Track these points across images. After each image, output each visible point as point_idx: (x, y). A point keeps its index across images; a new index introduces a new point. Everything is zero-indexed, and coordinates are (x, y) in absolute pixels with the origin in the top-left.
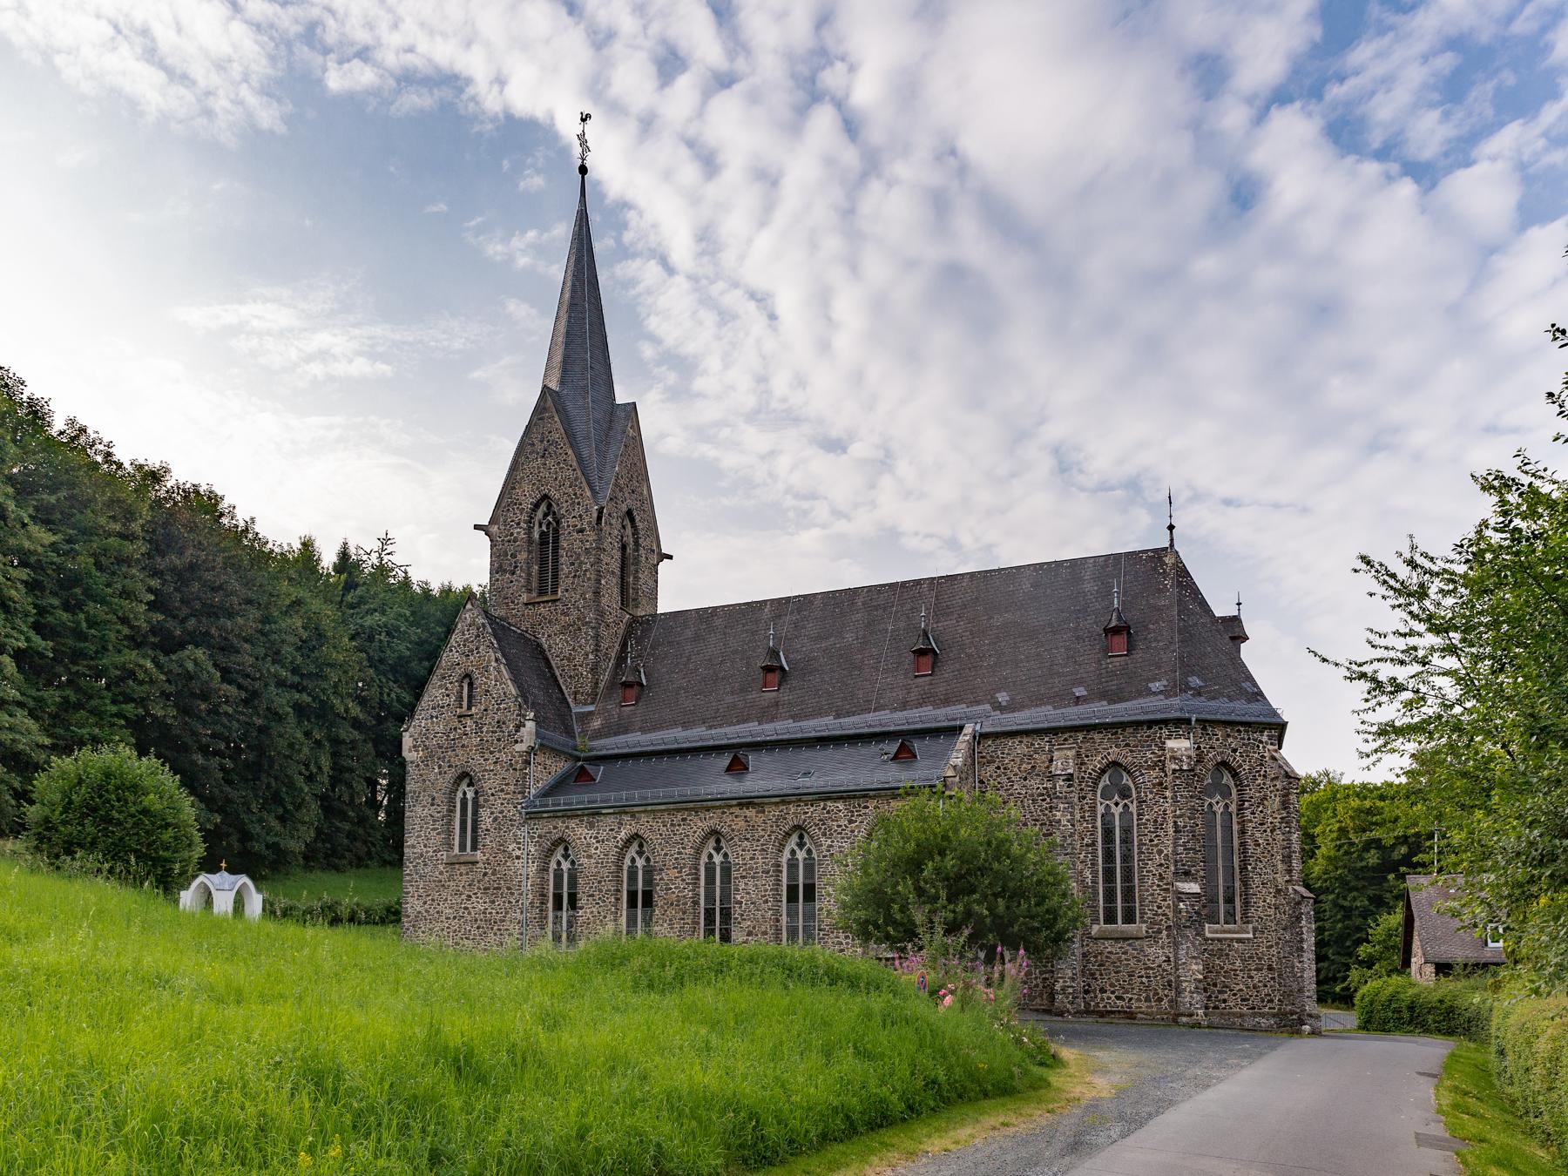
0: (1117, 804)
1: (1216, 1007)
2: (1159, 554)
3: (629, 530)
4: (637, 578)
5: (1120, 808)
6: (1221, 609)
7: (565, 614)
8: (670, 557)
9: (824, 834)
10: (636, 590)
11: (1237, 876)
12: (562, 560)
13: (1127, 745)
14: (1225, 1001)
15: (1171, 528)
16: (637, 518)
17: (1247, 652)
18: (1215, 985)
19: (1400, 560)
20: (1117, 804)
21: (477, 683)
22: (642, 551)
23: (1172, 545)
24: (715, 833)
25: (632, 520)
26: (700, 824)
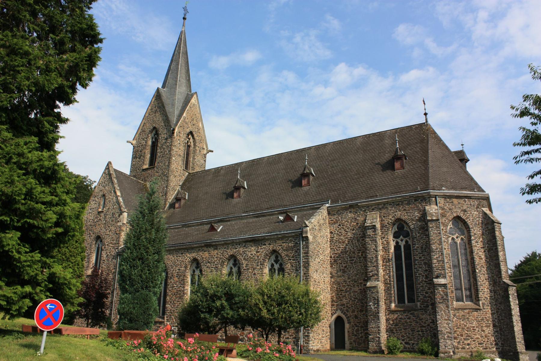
0: (402, 240)
1: (463, 348)
2: (421, 125)
3: (191, 140)
4: (194, 159)
5: (404, 243)
6: (454, 147)
7: (157, 172)
8: (212, 151)
9: (245, 259)
10: (193, 164)
11: (471, 276)
12: (158, 151)
13: (405, 210)
14: (468, 344)
15: (426, 114)
16: (195, 135)
17: (470, 168)
18: (462, 335)
19: (526, 195)
20: (402, 240)
21: (107, 198)
22: (197, 148)
23: (427, 121)
24: (195, 260)
25: (193, 136)
26: (189, 257)
